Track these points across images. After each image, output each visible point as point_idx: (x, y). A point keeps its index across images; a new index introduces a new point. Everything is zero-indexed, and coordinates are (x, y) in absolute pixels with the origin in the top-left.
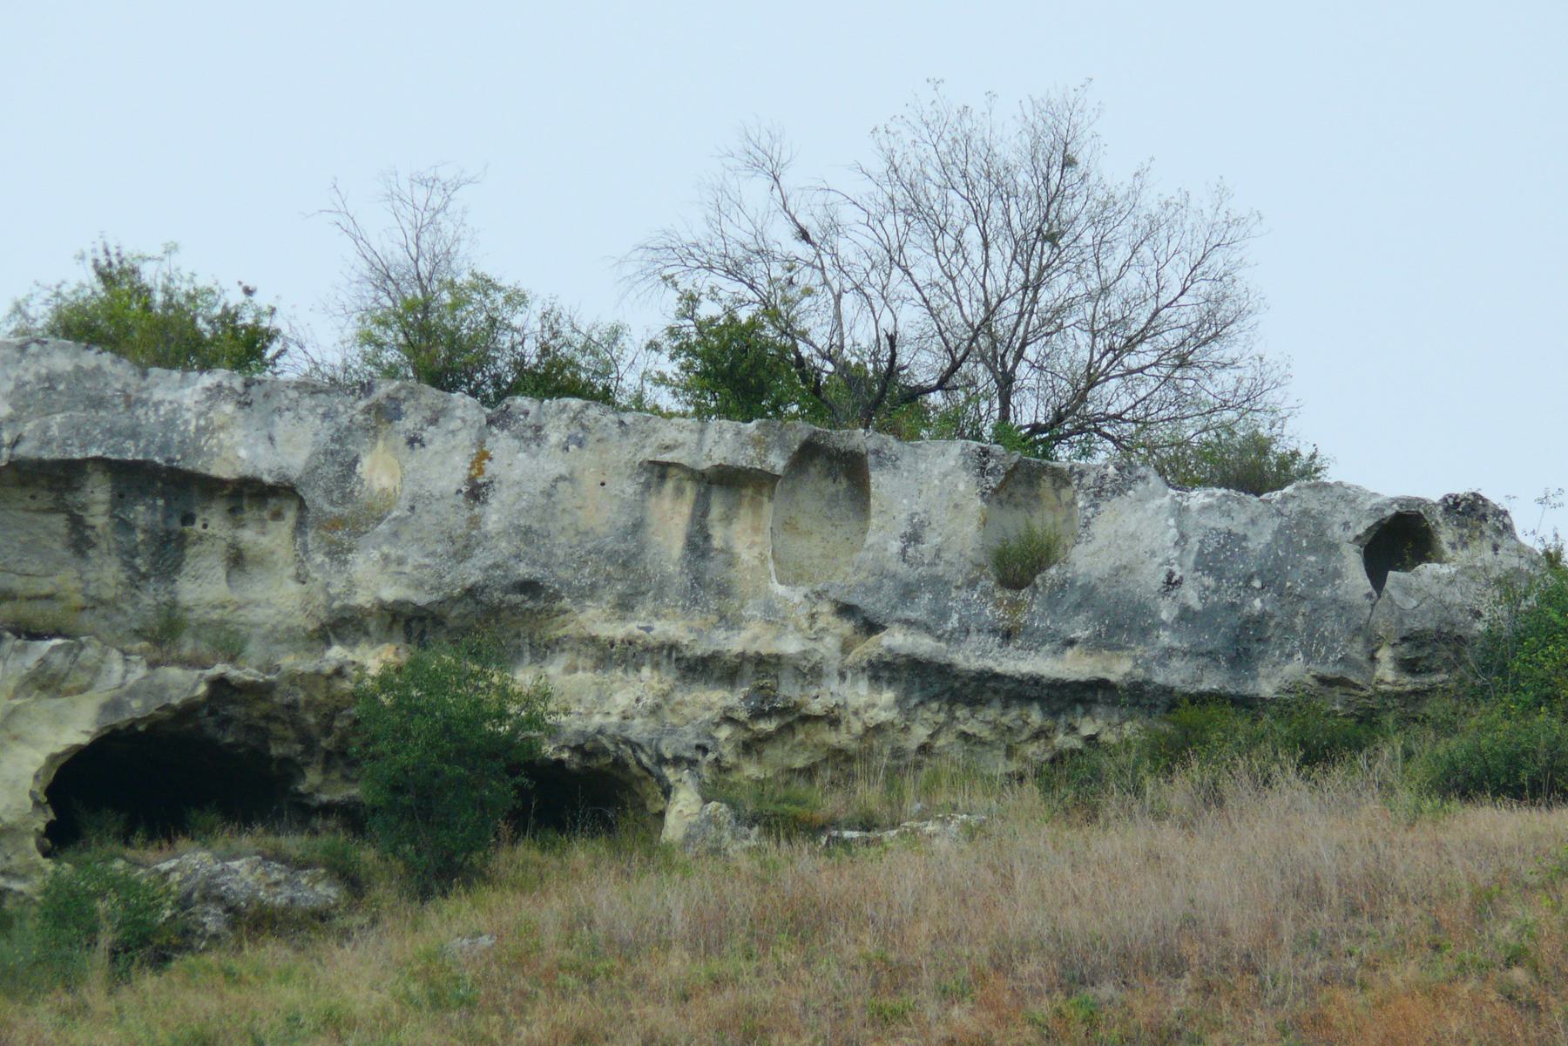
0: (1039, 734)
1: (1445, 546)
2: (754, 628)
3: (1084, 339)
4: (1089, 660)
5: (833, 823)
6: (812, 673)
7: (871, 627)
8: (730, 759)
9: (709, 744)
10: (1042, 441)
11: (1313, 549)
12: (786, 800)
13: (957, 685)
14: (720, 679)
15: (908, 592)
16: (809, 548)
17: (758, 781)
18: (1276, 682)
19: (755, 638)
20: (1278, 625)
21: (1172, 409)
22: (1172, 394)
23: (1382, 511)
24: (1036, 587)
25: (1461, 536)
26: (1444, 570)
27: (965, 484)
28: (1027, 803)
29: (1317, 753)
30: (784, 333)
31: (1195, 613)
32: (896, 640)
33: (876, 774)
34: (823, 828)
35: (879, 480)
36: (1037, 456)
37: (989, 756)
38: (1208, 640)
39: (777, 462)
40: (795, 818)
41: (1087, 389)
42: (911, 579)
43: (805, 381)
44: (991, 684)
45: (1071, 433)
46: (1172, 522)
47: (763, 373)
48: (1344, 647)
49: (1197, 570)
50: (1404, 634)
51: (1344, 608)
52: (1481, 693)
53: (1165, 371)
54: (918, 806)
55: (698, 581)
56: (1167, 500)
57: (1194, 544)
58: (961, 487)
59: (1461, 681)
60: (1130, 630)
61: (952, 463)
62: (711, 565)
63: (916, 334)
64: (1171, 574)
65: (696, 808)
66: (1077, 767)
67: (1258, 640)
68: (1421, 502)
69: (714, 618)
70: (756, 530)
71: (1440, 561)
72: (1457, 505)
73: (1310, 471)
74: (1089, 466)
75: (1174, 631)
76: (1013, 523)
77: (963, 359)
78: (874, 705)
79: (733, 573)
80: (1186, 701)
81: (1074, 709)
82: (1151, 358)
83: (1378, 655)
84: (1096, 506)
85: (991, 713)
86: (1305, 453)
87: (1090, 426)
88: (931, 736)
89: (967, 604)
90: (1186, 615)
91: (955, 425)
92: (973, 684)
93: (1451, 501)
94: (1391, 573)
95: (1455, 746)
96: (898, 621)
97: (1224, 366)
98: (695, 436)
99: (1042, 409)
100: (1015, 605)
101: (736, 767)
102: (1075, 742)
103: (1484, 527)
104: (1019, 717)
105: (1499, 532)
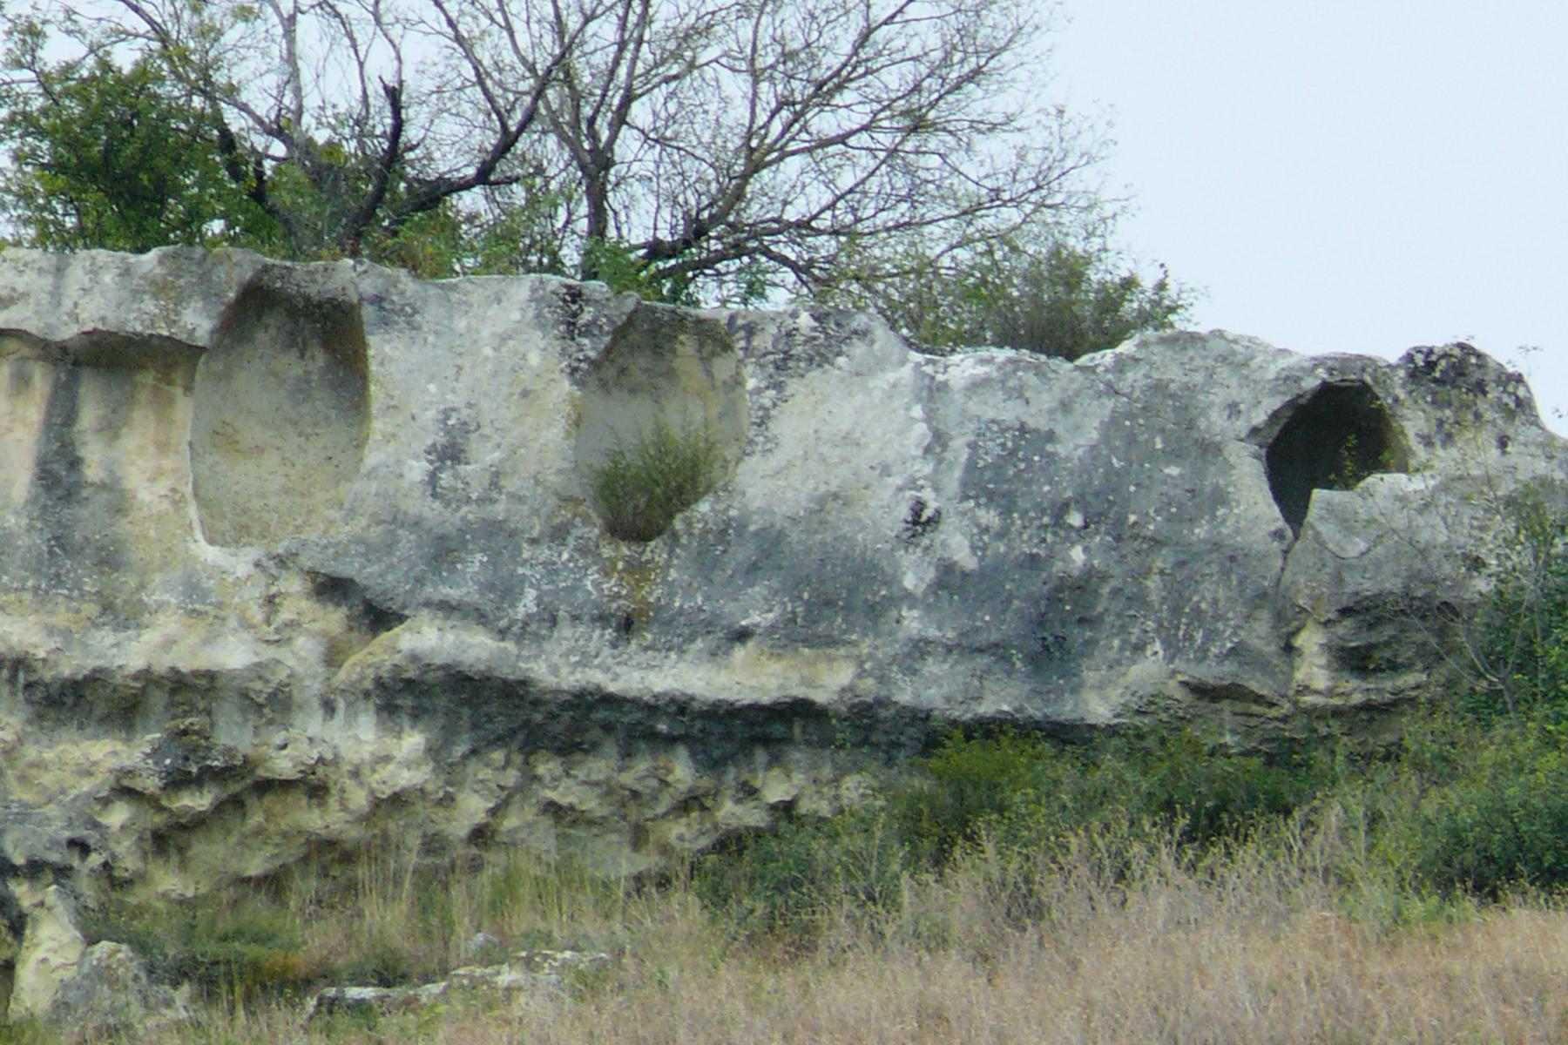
0: (690, 803)
1: (1413, 442)
2: (167, 625)
3: (736, 86)
4: (775, 667)
5: (327, 975)
6: (272, 703)
7: (379, 617)
8: (129, 863)
9: (92, 837)
10: (665, 274)
11: (1174, 454)
12: (239, 934)
13: (538, 717)
14: (105, 720)
15: (443, 552)
16: (256, 478)
17: (182, 902)
18: (1116, 695)
19: (169, 643)
20: (1116, 592)
21: (904, 206)
22: (901, 182)
23: (1297, 380)
24: (675, 536)
25: (1441, 423)
26: (1413, 485)
27: (540, 353)
28: (681, 926)
29: (1211, 821)
30: (194, 89)
31: (965, 575)
32: (426, 639)
33: (397, 883)
34: (305, 984)
35: (385, 351)
36: (662, 299)
37: (599, 844)
38: (991, 625)
39: (197, 322)
40: (255, 966)
41: (745, 177)
42: (448, 528)
43: (236, 175)
44: (600, 715)
45: (722, 256)
46: (917, 411)
47: (162, 163)
48: (1237, 627)
49: (966, 497)
50: (1345, 602)
51: (1233, 559)
52: (1487, 708)
53: (886, 140)
54: (480, 938)
55: (61, 543)
56: (906, 372)
57: (959, 451)
58: (534, 359)
59: (1450, 684)
60: (848, 608)
61: (516, 316)
62: (84, 513)
63: (429, 85)
64: (919, 506)
65: (73, 954)
66: (769, 858)
67: (1081, 621)
68: (1365, 362)
69: (91, 609)
70: (163, 447)
71: (1403, 468)
72: (1431, 366)
73: (1158, 313)
74: (764, 316)
75: (929, 608)
76: (631, 422)
77: (523, 127)
78: (387, 759)
79: (123, 526)
80: (958, 734)
81: (749, 756)
82: (860, 117)
83: (1298, 642)
84: (779, 386)
85: (599, 767)
86: (1148, 281)
87: (747, 243)
88: (493, 812)
89: (551, 569)
90: (948, 578)
91: (511, 248)
92: (567, 716)
93: (1420, 360)
94: (1318, 494)
95: (1461, 801)
96: (427, 604)
97: (993, 127)
98: (48, 281)
99: (666, 213)
100: (637, 569)
101: (140, 878)
102: (751, 816)
103: (1482, 405)
104: (653, 772)
105: (1510, 415)
